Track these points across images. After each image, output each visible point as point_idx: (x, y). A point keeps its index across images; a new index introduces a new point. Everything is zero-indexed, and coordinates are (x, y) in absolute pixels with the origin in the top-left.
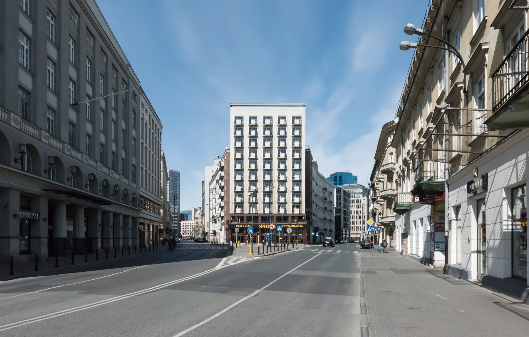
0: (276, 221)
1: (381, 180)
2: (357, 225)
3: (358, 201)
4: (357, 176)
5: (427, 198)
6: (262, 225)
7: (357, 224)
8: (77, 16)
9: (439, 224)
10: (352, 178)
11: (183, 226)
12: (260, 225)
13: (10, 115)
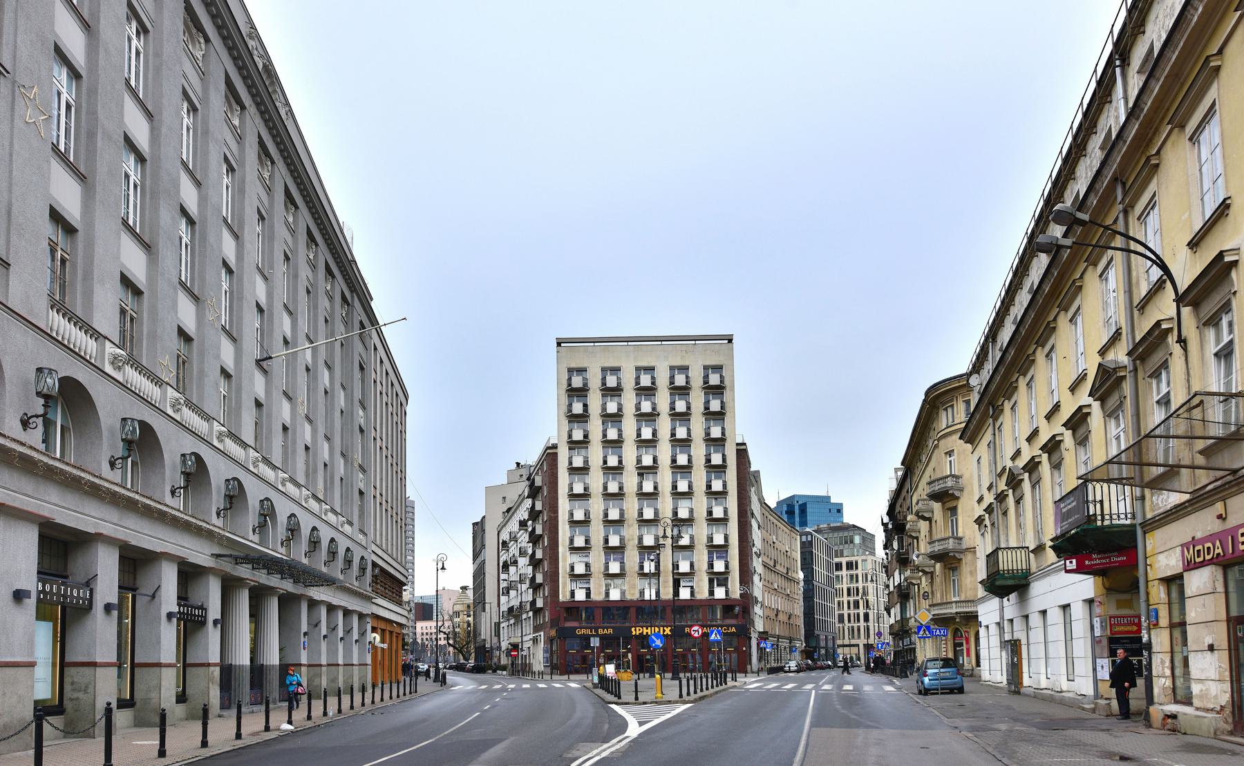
0: (637, 618)
1: (926, 515)
2: (850, 625)
3: (850, 566)
4: (841, 504)
5: (1095, 562)
6: (637, 629)
7: (849, 621)
8: (269, 163)
9: (1117, 617)
10: (830, 510)
11: (422, 634)
12: (633, 629)
13: (166, 392)
